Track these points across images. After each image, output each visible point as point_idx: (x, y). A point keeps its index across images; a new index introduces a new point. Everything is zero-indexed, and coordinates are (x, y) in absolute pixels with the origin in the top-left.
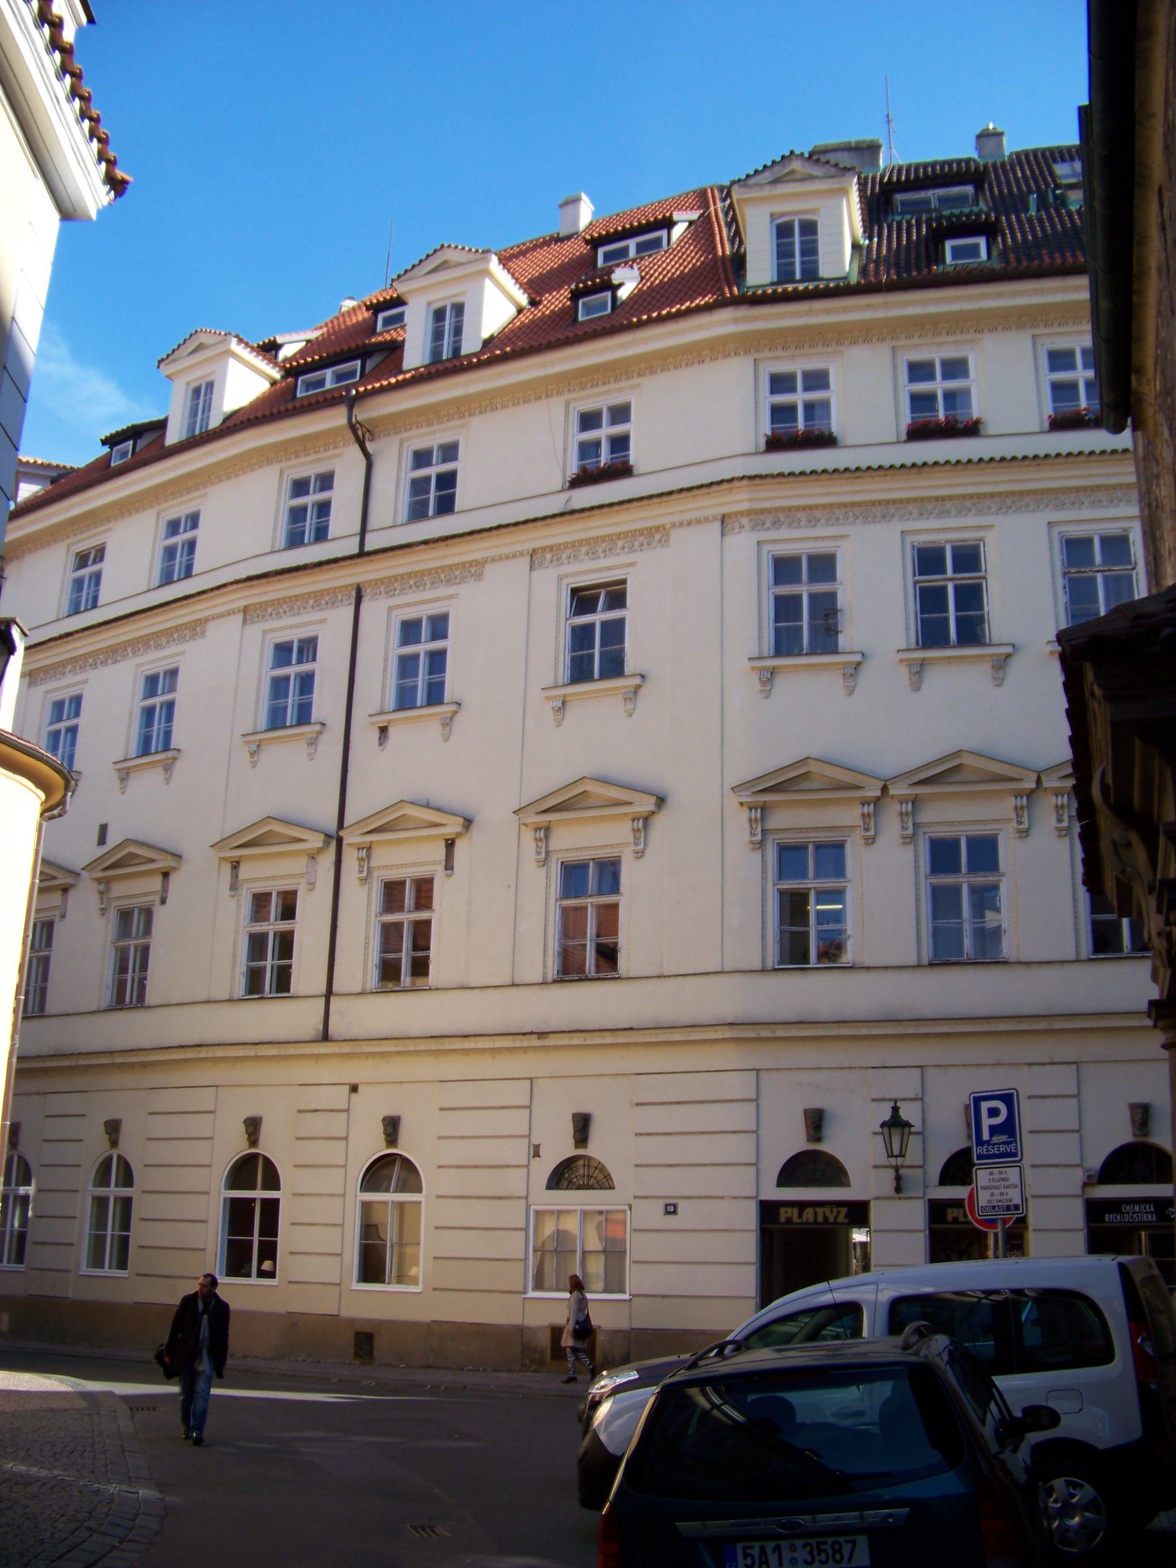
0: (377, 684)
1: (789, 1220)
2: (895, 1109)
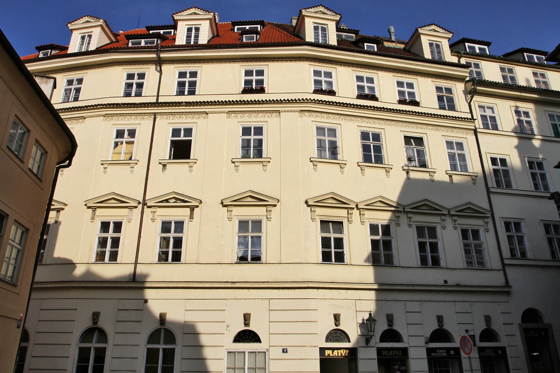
0: (163, 149)
1: (329, 355)
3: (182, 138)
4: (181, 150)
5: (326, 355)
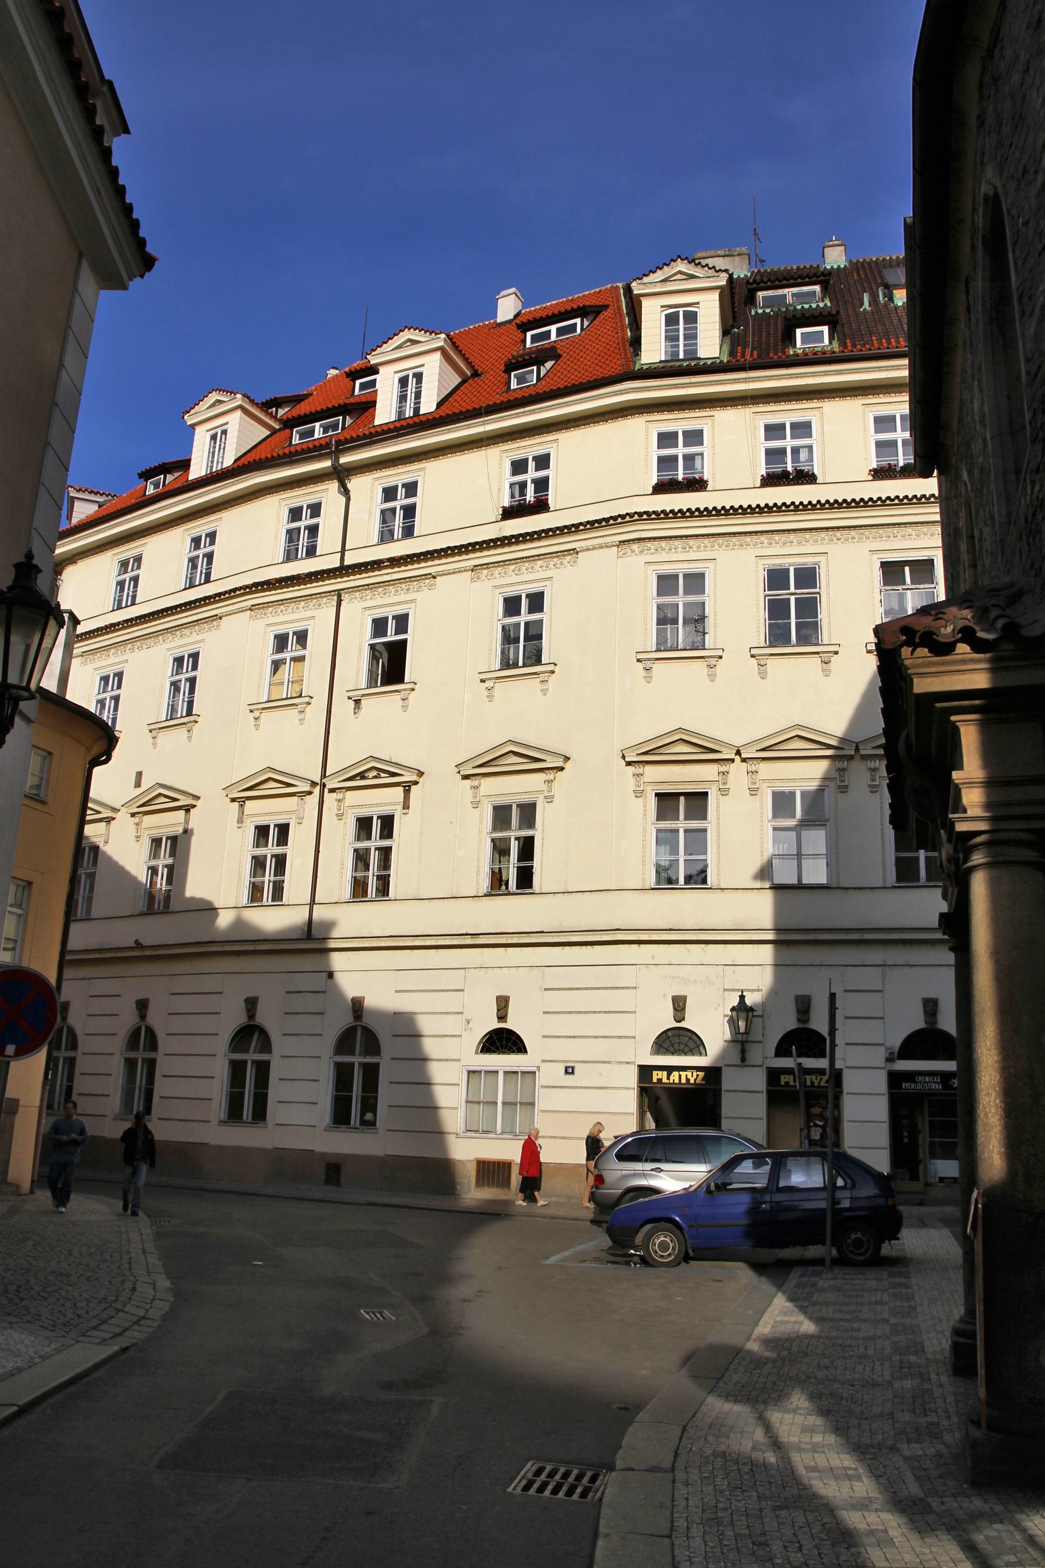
0: (355, 664)
2: (742, 997)
3: (391, 637)
4: (391, 664)
5: (655, 1080)
